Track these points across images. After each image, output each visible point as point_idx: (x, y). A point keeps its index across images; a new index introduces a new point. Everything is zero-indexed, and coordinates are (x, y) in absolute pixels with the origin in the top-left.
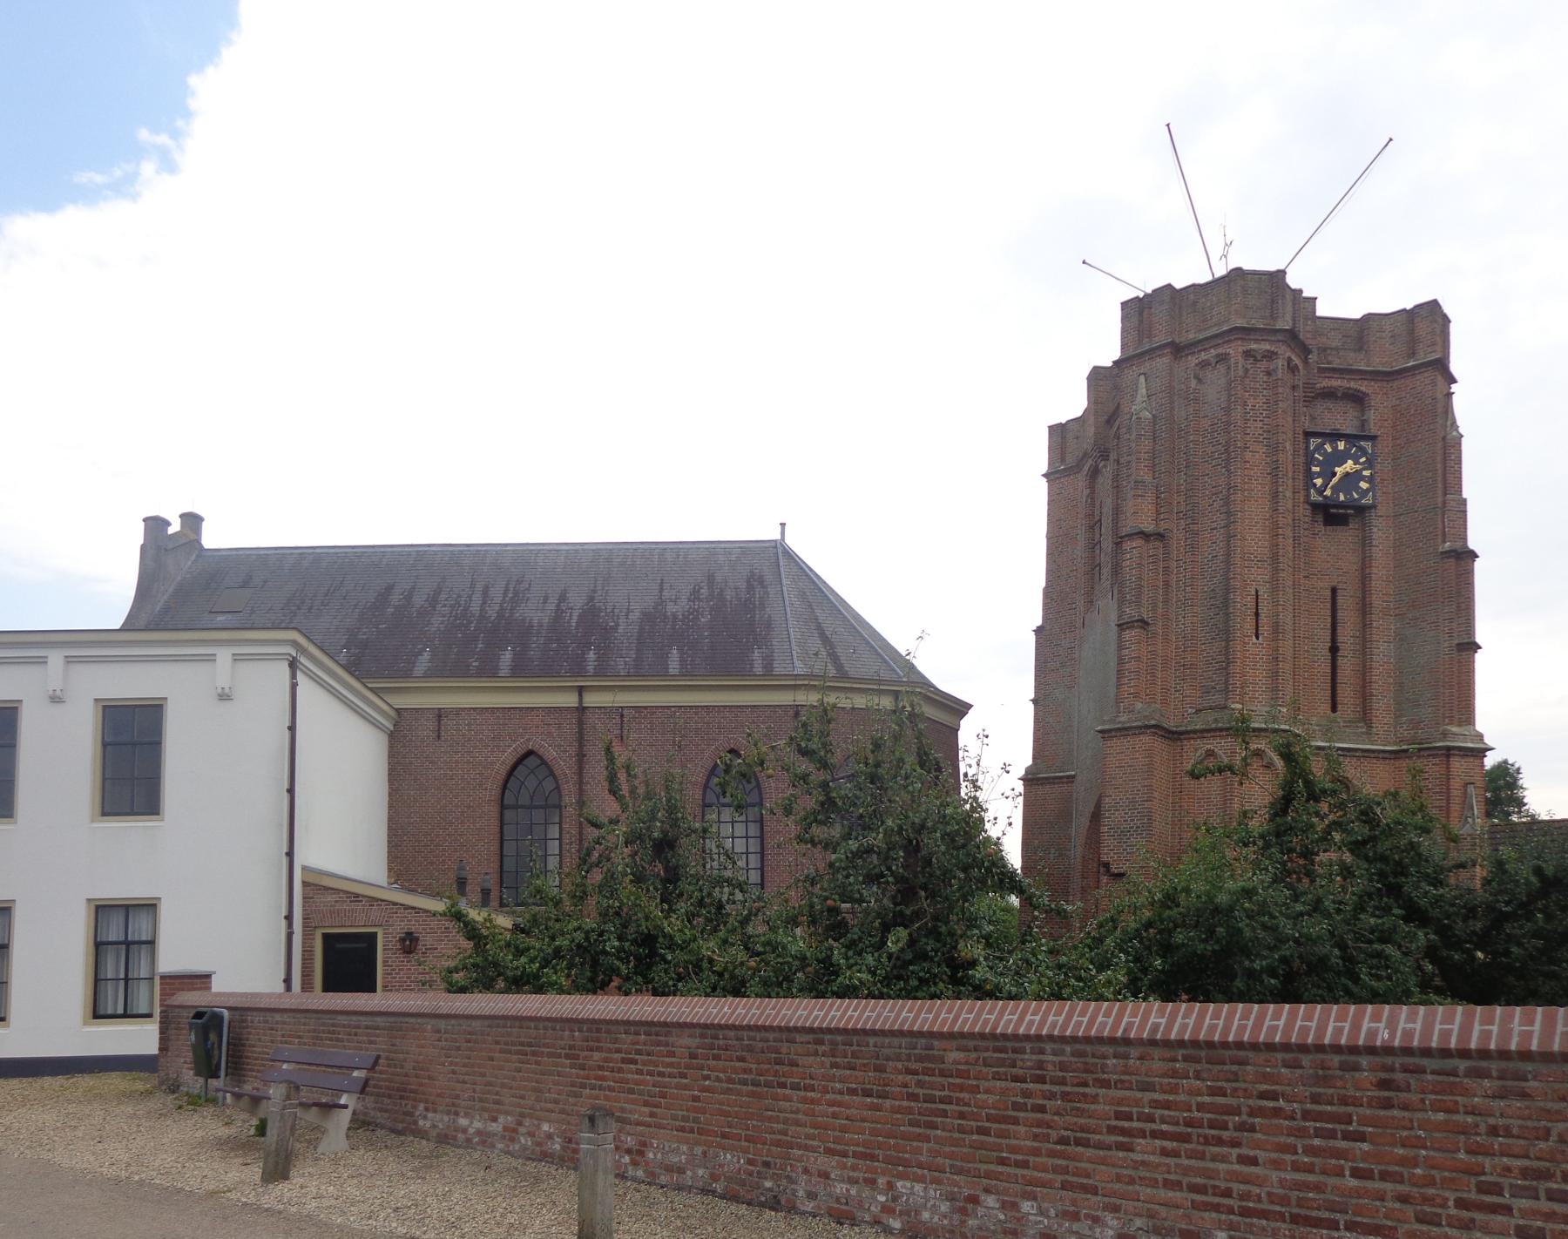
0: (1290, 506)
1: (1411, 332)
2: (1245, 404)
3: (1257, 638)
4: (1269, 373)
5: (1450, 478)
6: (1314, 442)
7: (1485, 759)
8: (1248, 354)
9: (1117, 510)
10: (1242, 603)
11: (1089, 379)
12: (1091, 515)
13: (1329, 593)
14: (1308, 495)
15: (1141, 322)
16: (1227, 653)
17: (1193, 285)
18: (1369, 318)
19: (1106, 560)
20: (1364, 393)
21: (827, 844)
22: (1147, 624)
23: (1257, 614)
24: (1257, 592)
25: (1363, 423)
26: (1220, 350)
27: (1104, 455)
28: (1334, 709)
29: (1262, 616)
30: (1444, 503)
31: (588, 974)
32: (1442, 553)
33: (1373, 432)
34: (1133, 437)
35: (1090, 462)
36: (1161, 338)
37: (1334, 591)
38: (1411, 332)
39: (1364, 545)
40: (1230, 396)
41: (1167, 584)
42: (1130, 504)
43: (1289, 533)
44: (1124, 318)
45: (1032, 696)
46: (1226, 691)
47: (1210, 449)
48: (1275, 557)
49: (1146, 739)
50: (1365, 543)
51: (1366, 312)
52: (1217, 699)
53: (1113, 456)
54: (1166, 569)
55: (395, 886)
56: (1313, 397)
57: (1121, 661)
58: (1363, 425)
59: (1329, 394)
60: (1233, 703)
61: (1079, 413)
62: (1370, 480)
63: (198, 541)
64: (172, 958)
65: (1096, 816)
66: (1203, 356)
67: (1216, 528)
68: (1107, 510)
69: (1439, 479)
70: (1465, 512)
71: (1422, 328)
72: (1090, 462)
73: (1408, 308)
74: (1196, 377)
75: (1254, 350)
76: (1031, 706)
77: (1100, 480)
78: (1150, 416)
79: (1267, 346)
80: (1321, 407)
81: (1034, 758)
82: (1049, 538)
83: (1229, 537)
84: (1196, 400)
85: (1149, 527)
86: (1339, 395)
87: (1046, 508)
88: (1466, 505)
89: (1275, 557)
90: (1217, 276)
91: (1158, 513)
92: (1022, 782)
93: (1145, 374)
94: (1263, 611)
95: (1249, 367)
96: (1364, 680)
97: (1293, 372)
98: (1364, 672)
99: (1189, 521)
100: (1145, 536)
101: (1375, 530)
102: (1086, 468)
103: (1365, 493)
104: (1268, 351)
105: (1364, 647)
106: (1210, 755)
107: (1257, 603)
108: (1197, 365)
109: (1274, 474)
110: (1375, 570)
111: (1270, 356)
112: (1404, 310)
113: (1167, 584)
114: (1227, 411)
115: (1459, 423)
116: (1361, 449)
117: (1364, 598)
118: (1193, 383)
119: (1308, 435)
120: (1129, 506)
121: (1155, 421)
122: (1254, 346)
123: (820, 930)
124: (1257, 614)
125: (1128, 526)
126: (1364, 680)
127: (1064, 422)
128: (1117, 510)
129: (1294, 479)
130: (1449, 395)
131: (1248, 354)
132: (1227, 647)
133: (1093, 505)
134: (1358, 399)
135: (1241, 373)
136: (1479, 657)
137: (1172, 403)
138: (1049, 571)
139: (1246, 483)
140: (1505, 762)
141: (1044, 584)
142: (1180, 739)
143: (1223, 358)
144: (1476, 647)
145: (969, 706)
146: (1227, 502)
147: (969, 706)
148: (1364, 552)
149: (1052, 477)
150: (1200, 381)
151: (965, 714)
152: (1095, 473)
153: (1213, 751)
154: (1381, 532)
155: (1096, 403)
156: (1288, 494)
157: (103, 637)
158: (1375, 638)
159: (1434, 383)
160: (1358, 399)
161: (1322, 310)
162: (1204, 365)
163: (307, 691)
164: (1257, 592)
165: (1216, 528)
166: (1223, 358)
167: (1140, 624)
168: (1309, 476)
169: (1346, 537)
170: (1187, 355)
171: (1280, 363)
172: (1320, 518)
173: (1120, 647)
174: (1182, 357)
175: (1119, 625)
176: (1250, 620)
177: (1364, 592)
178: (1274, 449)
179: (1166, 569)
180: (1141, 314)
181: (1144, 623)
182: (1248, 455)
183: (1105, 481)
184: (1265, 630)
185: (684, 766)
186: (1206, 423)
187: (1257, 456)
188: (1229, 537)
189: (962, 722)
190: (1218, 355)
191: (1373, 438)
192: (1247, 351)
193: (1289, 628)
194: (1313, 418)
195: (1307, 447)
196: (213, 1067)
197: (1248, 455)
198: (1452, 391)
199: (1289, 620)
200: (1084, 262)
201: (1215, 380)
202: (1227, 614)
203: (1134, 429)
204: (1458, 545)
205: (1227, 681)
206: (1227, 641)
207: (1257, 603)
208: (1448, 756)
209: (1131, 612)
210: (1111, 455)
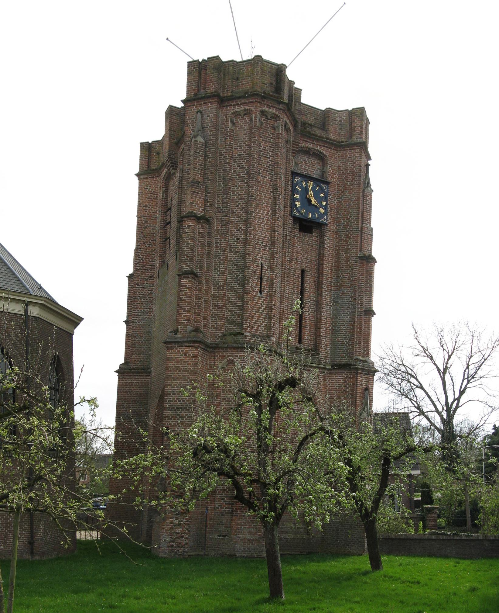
0: (282, 215)
1: (351, 124)
2: (260, 146)
3: (261, 293)
4: (274, 129)
5: (366, 214)
6: (297, 179)
7: (374, 376)
8: (263, 113)
9: (180, 203)
10: (253, 269)
11: (166, 113)
12: (164, 205)
13: (300, 272)
14: (292, 211)
15: (200, 77)
16: (243, 301)
17: (232, 61)
18: (329, 111)
19: (172, 235)
20: (325, 155)
21: (210, 228)
22: (197, 276)
23: (261, 278)
24: (262, 264)
25: (323, 173)
26: (247, 107)
27: (174, 166)
28: (300, 342)
29: (264, 280)
30: (362, 228)
31: (325, 486)
32: (359, 257)
33: (329, 179)
34: (192, 153)
35: (166, 170)
36: (211, 90)
37: (303, 271)
38: (351, 124)
39: (320, 247)
40: (251, 138)
41: (209, 252)
42: (189, 197)
43: (281, 231)
44: (190, 73)
45: (125, 319)
46: (242, 324)
47: (238, 170)
48: (272, 245)
49: (193, 350)
50: (321, 245)
51: (328, 107)
52: (236, 329)
53: (180, 166)
54: (209, 243)
55: (364, 148)
56: (296, 151)
57: (179, 298)
58: (323, 175)
59: (307, 152)
60: (245, 331)
61: (160, 138)
62: (325, 208)
63: (222, 61)
64: (180, 105)
65: (162, 398)
66: (237, 109)
67: (239, 221)
68: (175, 202)
69: (360, 214)
70: (371, 235)
71: (356, 123)
72: (166, 170)
73: (349, 110)
74: (232, 122)
75: (266, 111)
76: (124, 326)
77: (172, 183)
78: (203, 141)
79: (243, 108)
80: (301, 158)
81: (126, 358)
82: (138, 217)
83: (247, 227)
84: (231, 136)
85: (199, 212)
86: (311, 153)
87: (137, 196)
88: (372, 231)
89: (272, 245)
90: (245, 59)
91: (206, 206)
92: (117, 374)
93: (201, 113)
94: (265, 277)
95: (263, 122)
96: (316, 326)
97: (288, 132)
98: (317, 321)
99: (224, 214)
100: (198, 219)
101: (326, 238)
102: (163, 174)
103: (323, 215)
104: (275, 114)
105: (317, 307)
106: (231, 363)
107: (261, 272)
108: (232, 114)
109: (275, 189)
110: (325, 263)
111: (276, 117)
112: (347, 110)
113: (209, 252)
114: (249, 147)
115: (371, 183)
116: (321, 188)
117: (319, 278)
118: (230, 125)
119: (294, 174)
120: (188, 199)
121: (206, 145)
122: (266, 109)
123: (98, 512)
124: (261, 278)
125: (187, 210)
126: (316, 326)
127: (150, 142)
128: (180, 203)
129: (285, 198)
130: (368, 165)
131: (263, 113)
132: (243, 297)
133: (166, 199)
134: (321, 157)
135: (258, 124)
136: (375, 320)
137: (217, 135)
138: (138, 239)
139: (258, 195)
140: (375, 314)
141: (134, 247)
142: (214, 352)
143: (248, 112)
144: (374, 261)
145: (81, 319)
146: (247, 205)
147: (81, 319)
148: (320, 251)
149: (142, 177)
150: (234, 124)
151: (147, 143)
152: (168, 178)
153: (233, 360)
154: (329, 240)
155: (170, 130)
156: (282, 207)
157: (61, 309)
158: (323, 302)
159: (360, 156)
160: (321, 157)
161: (304, 100)
162: (236, 114)
163: (75, 404)
164: (262, 264)
165: (239, 221)
166: (248, 112)
167: (192, 275)
168: (294, 200)
169: (311, 239)
170: (227, 106)
171: (281, 124)
172: (297, 226)
173: (180, 289)
174: (224, 106)
175: (179, 275)
176: (257, 281)
177: (319, 275)
178: (275, 177)
179: (209, 243)
180: (200, 73)
181: (194, 275)
182: (260, 178)
183: (174, 184)
184: (265, 289)
185: (56, 493)
186: (236, 153)
187: (265, 179)
188: (247, 227)
189: (76, 330)
190: (245, 110)
191: (328, 183)
192: (262, 111)
193: (278, 290)
194: (296, 164)
195: (293, 182)
196: (450, 405)
197: (260, 178)
198: (183, 105)
199: (278, 284)
200: (167, 39)
201: (243, 123)
202: (244, 276)
203: (192, 148)
204: (367, 254)
205: (242, 318)
206: (244, 293)
207: (261, 272)
208: (357, 373)
209: (186, 267)
210: (179, 167)
